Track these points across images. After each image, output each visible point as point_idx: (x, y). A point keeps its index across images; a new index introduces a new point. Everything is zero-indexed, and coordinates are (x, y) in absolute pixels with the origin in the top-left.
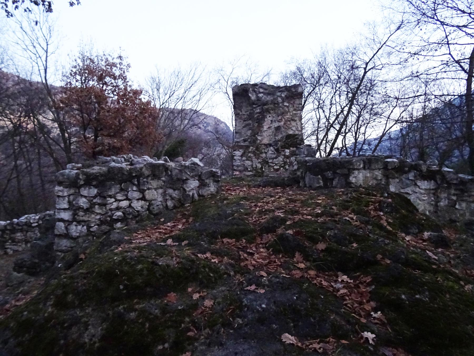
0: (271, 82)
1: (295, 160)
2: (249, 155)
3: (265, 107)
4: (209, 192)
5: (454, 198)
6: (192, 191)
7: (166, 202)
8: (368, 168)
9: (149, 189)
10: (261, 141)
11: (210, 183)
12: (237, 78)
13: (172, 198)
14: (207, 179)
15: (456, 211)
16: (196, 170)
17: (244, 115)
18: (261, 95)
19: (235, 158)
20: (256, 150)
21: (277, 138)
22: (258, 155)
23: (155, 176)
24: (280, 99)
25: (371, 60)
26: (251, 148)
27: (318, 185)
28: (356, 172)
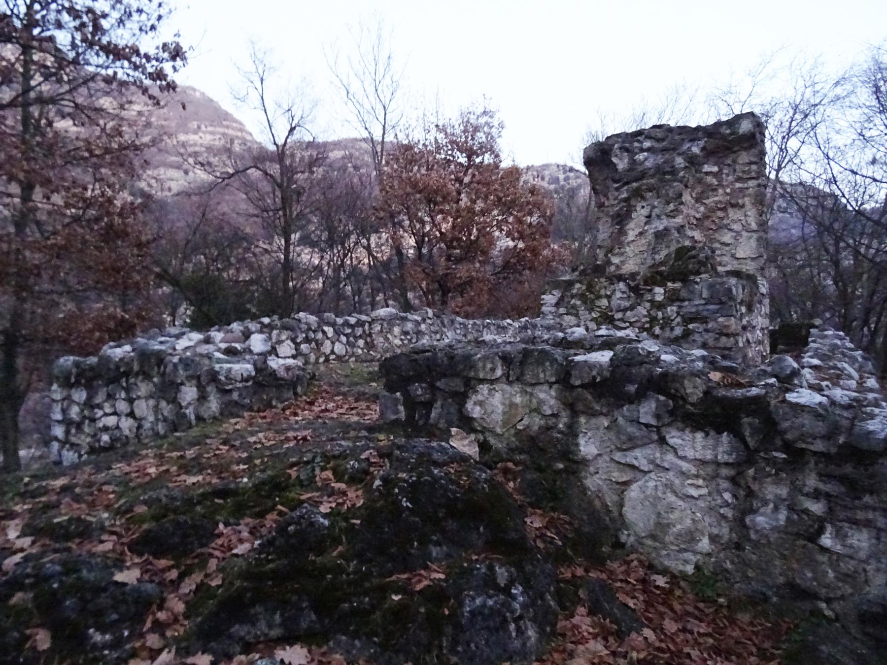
1: (678, 313)
2: (573, 301)
5: (816, 508)
8: (518, 379)
15: (823, 558)
18: (641, 157)
19: (544, 309)
20: (588, 289)
21: (657, 257)
22: (593, 301)
26: (578, 285)
27: (393, 417)
28: (484, 389)
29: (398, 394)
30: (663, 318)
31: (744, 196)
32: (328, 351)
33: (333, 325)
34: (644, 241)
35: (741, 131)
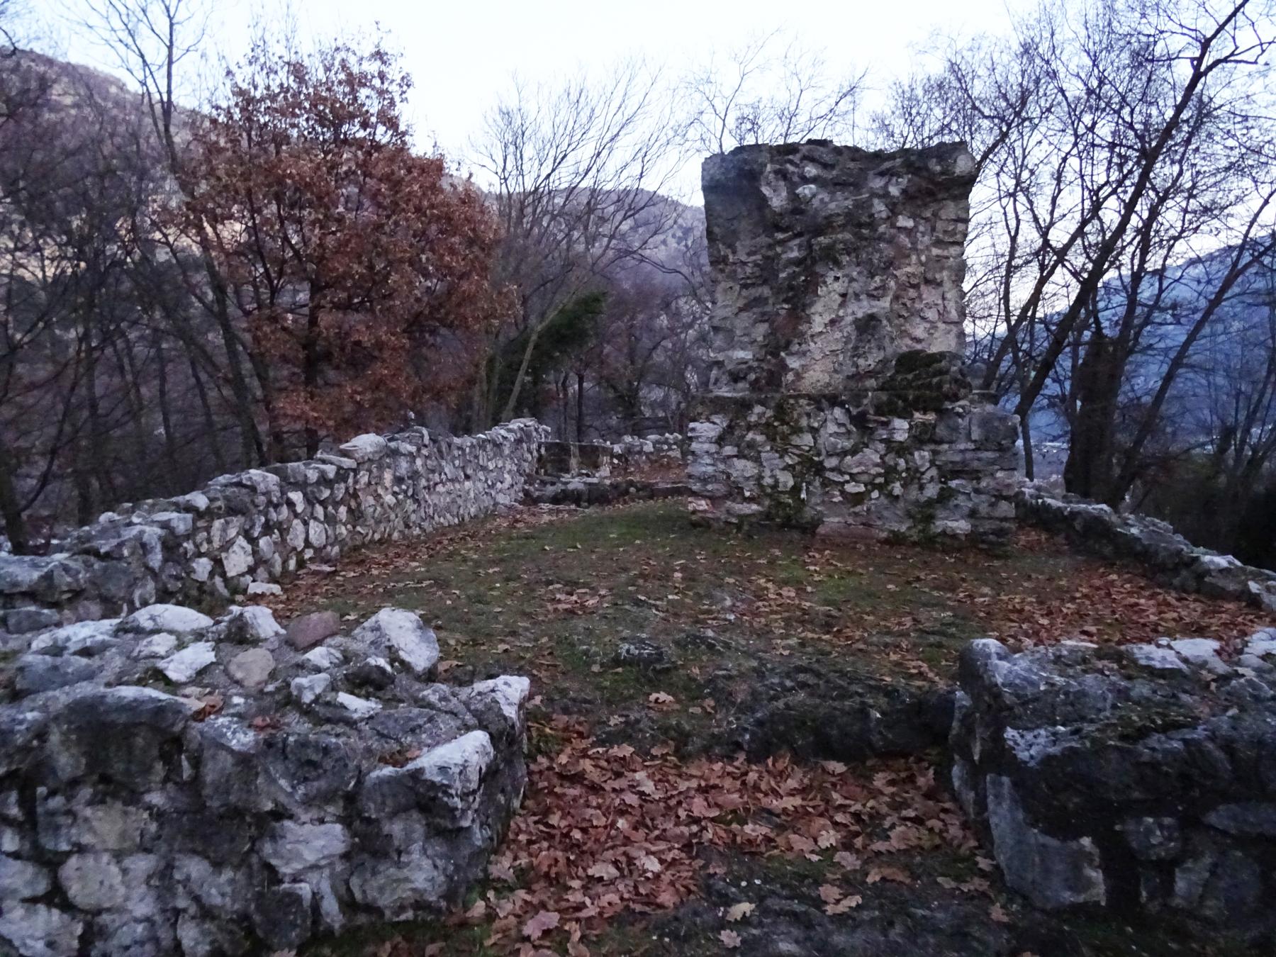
0: (842, 139)
1: (932, 463)
2: (750, 436)
3: (821, 239)
4: (404, 893)
6: (314, 877)
7: (174, 926)
9: (81, 849)
10: (799, 376)
11: (409, 840)
12: (755, 108)
13: (206, 913)
14: (393, 815)
16: (328, 764)
17: (745, 264)
18: (806, 190)
19: (694, 446)
21: (861, 362)
22: (785, 438)
23: (115, 788)
24: (879, 208)
25: (1221, 28)
26: (758, 409)
27: (1068, 897)
29: (1086, 841)
30: (908, 470)
31: (942, 269)
32: (300, 544)
33: (302, 485)
34: (838, 335)
35: (958, 171)
